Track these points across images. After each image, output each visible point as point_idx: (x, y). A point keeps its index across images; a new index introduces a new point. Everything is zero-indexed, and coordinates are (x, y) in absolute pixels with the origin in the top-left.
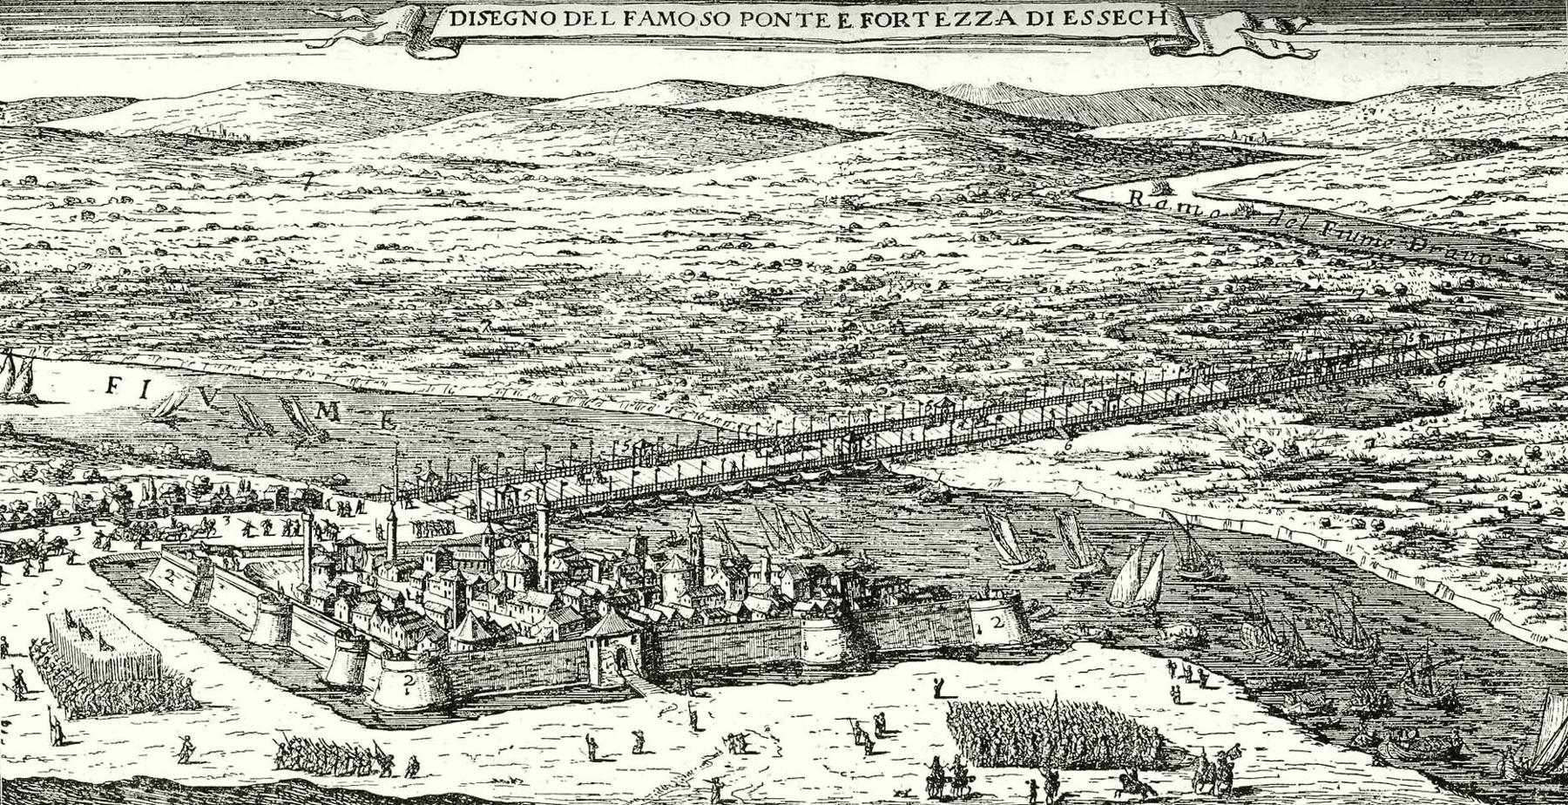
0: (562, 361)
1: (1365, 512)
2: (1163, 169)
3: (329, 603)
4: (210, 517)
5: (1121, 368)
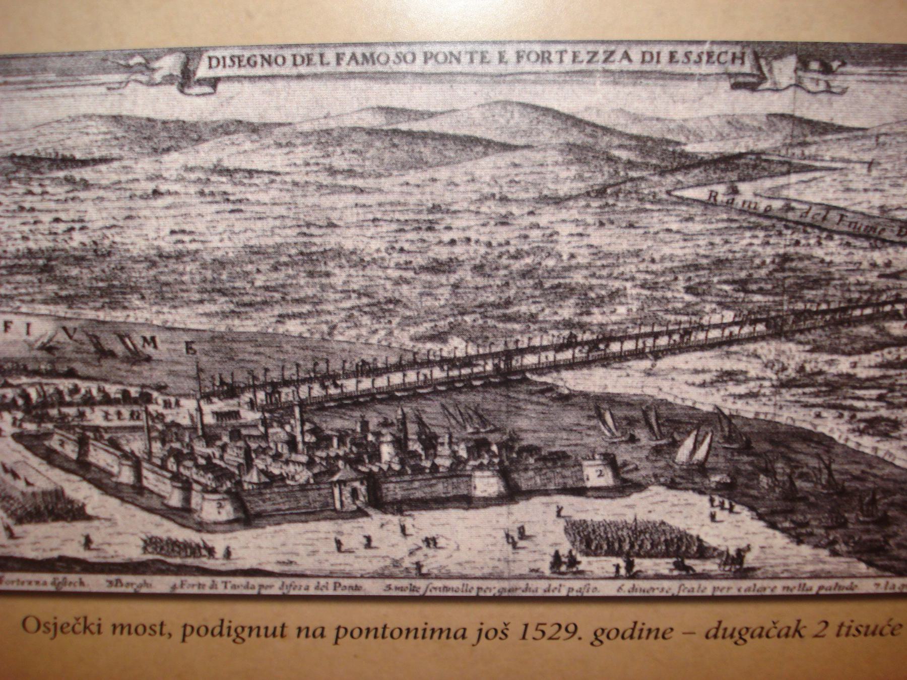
0: (306, 308)
1: (845, 408)
2: (733, 176)
3: (164, 460)
4: (81, 409)
5: (694, 314)
